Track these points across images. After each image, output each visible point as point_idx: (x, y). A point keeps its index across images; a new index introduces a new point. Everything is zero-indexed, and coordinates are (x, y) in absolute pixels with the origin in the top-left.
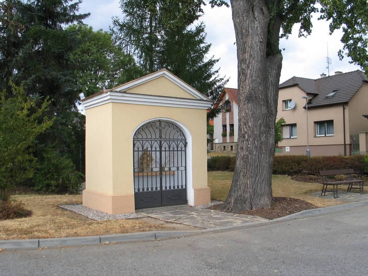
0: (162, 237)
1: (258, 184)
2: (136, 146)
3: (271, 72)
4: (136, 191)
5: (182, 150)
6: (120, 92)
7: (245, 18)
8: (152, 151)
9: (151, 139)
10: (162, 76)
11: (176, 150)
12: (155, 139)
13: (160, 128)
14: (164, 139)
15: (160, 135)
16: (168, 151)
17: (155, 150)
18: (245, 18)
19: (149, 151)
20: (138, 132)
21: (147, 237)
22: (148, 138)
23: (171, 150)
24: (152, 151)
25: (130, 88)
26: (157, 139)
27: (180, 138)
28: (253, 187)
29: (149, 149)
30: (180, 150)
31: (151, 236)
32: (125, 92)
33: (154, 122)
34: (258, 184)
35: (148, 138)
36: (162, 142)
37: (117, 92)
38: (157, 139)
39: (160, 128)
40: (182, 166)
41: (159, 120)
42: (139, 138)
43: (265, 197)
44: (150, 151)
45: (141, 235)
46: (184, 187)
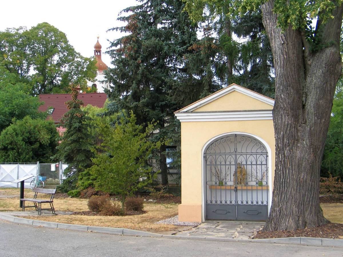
0: (128, 233)
1: (284, 202)
2: (209, 160)
3: (316, 72)
4: (209, 202)
5: (222, 164)
6: (184, 112)
7: (268, 21)
8: (246, 165)
9: (220, 153)
10: (233, 91)
11: (224, 164)
12: (219, 153)
13: (237, 142)
14: (240, 153)
15: (235, 149)
16: (260, 165)
17: (258, 164)
18: (268, 21)
19: (244, 165)
20: (208, 148)
21: (117, 232)
22: (221, 152)
23: (227, 163)
24: (246, 165)
25: (198, 107)
26: (232, 153)
27: (259, 151)
28: (279, 205)
29: (244, 163)
30: (220, 164)
31: (120, 232)
32: (192, 112)
33: (227, 136)
34: (284, 202)
35: (221, 152)
36: (238, 156)
37: (182, 113)
38: (232, 153)
39: (237, 142)
40: (252, 181)
41: (236, 134)
42: (212, 152)
43: (289, 218)
44: (245, 165)
45: (113, 229)
46: (265, 203)
